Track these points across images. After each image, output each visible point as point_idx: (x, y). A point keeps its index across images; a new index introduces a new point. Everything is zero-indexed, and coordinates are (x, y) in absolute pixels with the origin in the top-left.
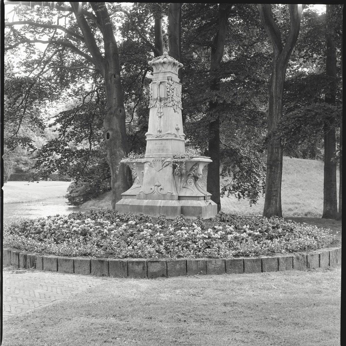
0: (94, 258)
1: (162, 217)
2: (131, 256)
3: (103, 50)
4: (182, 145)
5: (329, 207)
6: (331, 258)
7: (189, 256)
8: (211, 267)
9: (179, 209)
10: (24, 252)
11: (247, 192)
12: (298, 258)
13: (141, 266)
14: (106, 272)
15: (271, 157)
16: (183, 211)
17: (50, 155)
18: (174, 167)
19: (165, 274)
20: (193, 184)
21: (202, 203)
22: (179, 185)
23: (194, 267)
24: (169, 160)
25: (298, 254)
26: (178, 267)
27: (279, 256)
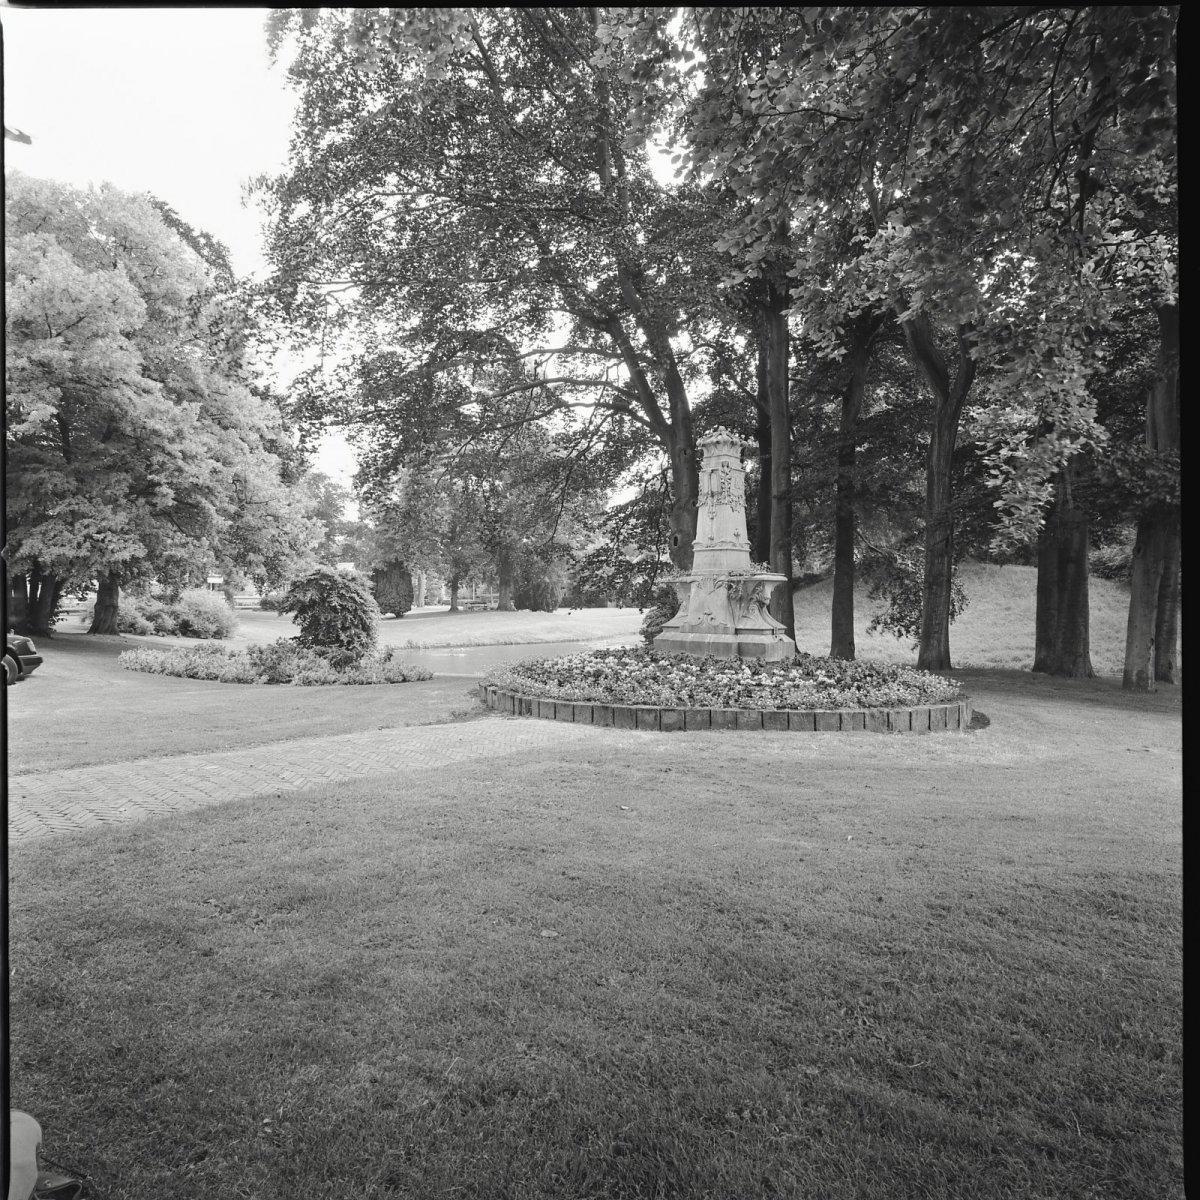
0: (598, 704)
1: (707, 657)
2: (645, 703)
3: (666, 415)
4: (746, 557)
5: (1043, 653)
6: (932, 718)
7: (717, 705)
8: (742, 720)
9: (734, 647)
10: (519, 695)
11: (913, 627)
12: (872, 716)
13: (652, 716)
14: (610, 721)
15: (930, 571)
16: (741, 650)
17: (598, 569)
18: (730, 587)
19: (682, 726)
20: (757, 612)
21: (767, 639)
22: (738, 613)
23: (720, 720)
24: (722, 578)
25: (874, 710)
26: (699, 718)
27: (843, 711)
